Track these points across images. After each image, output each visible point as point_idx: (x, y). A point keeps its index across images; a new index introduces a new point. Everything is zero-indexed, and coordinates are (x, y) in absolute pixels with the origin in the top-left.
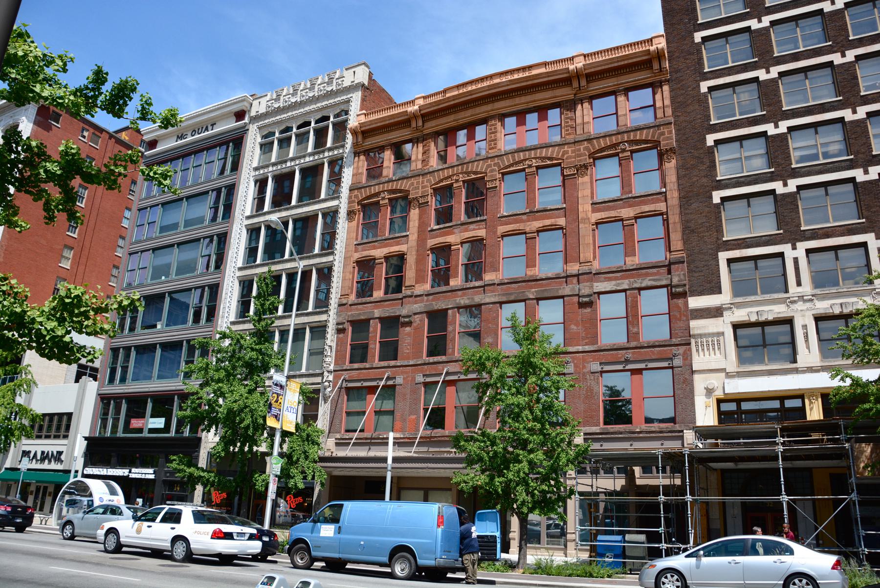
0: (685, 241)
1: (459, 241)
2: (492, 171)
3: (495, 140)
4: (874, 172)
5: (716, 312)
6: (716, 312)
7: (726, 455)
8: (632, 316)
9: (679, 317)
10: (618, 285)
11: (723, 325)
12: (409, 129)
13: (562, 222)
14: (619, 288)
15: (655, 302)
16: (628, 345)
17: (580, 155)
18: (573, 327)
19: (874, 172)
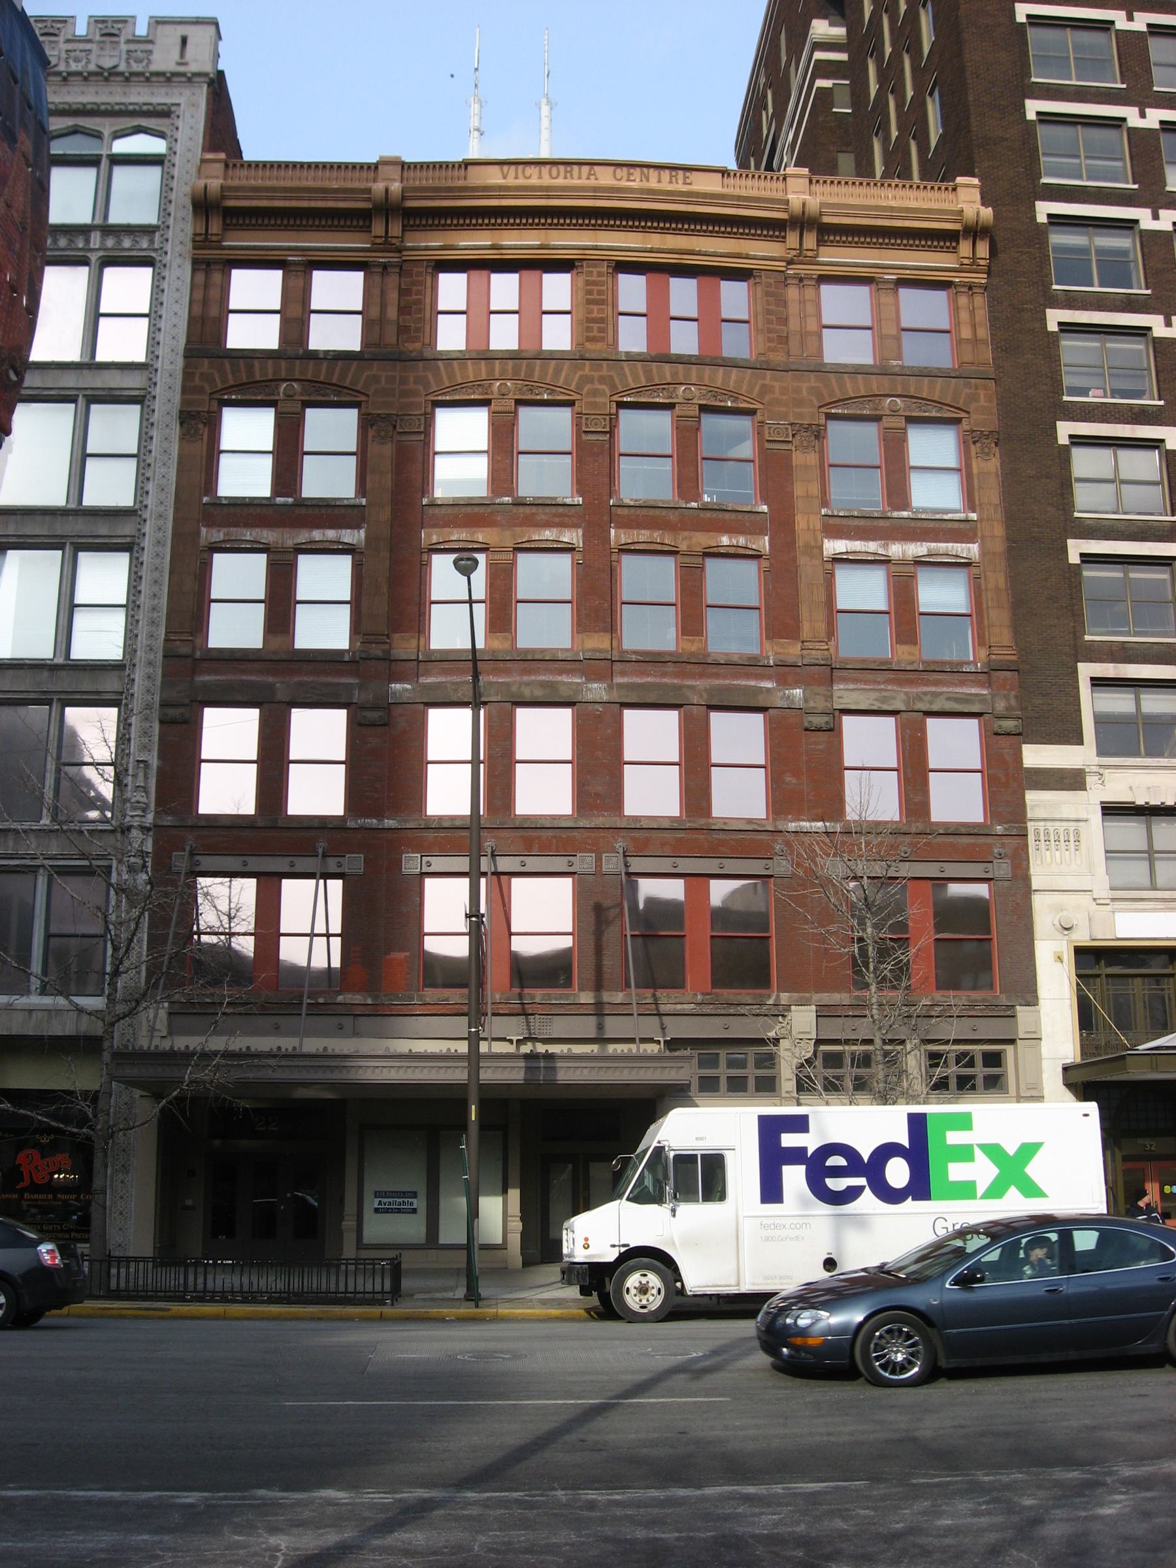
0: (1017, 628)
1: (510, 544)
2: (595, 393)
3: (589, 302)
4: (1166, 220)
5: (1073, 780)
6: (1073, 780)
7: (287, 228)
8: (914, 770)
9: (1006, 783)
10: (884, 700)
11: (1083, 806)
12: (364, 236)
13: (764, 544)
14: (885, 707)
15: (954, 743)
16: (905, 829)
17: (799, 403)
18: (788, 778)
19: (1166, 220)
